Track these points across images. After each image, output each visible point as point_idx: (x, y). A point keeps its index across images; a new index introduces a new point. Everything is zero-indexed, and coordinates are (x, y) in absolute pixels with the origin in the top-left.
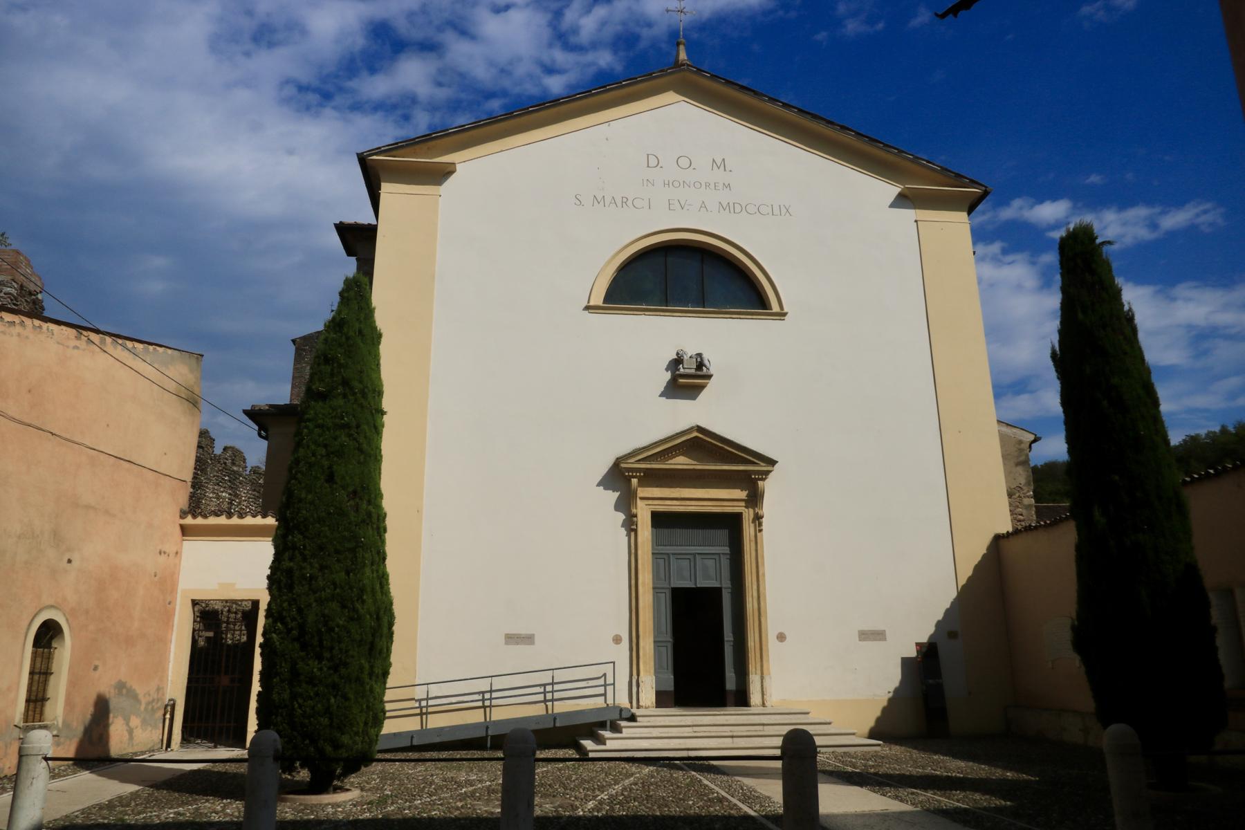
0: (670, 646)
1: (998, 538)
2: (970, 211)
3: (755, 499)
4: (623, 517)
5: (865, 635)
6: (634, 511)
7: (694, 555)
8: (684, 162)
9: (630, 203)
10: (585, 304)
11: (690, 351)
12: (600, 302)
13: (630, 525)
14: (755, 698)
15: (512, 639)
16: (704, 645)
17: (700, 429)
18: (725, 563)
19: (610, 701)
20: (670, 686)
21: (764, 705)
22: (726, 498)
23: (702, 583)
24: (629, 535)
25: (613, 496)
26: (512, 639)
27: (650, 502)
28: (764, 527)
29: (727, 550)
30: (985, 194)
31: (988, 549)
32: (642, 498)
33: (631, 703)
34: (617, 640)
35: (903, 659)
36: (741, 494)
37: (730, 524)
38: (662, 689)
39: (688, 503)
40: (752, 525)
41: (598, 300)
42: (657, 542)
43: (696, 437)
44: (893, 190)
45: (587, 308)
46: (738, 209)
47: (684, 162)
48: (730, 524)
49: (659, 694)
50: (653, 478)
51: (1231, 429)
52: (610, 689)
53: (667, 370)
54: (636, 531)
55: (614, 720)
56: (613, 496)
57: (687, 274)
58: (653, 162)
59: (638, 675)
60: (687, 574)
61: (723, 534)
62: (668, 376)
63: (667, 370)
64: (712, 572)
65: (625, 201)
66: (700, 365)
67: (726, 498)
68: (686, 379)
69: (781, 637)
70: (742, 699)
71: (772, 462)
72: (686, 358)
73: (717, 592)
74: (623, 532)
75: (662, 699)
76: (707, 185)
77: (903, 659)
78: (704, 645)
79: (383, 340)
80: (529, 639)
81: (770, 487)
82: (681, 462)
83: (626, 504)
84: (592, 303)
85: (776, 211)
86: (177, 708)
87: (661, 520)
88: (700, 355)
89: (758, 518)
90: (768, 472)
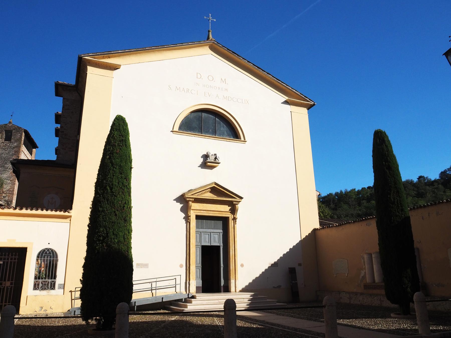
0: (200, 268)
1: (315, 230)
2: (308, 109)
3: (233, 211)
4: (184, 215)
7: (210, 233)
8: (211, 78)
9: (190, 91)
10: (172, 130)
11: (212, 153)
13: (187, 219)
14: (233, 289)
16: (214, 267)
17: (216, 184)
19: (178, 290)
20: (200, 285)
21: (236, 291)
24: (186, 223)
25: (180, 206)
27: (195, 211)
29: (221, 231)
30: (314, 105)
34: (181, 266)
36: (227, 208)
37: (225, 221)
38: (198, 286)
39: (209, 212)
40: (233, 221)
41: (176, 128)
42: (197, 227)
43: (214, 187)
44: (286, 98)
45: (172, 131)
46: (230, 99)
47: (211, 78)
48: (225, 221)
49: (197, 288)
50: (197, 201)
51: (344, 192)
53: (202, 157)
54: (190, 223)
55: (190, 298)
56: (180, 206)
57: (210, 122)
59: (189, 280)
61: (220, 223)
63: (202, 157)
64: (217, 240)
66: (216, 158)
67: (222, 210)
68: (207, 163)
71: (241, 198)
72: (210, 155)
73: (218, 247)
74: (184, 221)
76: (219, 88)
78: (214, 267)
81: (240, 207)
82: (209, 195)
83: (185, 210)
84: (174, 130)
85: (244, 102)
87: (198, 217)
88: (215, 154)
89: (234, 219)
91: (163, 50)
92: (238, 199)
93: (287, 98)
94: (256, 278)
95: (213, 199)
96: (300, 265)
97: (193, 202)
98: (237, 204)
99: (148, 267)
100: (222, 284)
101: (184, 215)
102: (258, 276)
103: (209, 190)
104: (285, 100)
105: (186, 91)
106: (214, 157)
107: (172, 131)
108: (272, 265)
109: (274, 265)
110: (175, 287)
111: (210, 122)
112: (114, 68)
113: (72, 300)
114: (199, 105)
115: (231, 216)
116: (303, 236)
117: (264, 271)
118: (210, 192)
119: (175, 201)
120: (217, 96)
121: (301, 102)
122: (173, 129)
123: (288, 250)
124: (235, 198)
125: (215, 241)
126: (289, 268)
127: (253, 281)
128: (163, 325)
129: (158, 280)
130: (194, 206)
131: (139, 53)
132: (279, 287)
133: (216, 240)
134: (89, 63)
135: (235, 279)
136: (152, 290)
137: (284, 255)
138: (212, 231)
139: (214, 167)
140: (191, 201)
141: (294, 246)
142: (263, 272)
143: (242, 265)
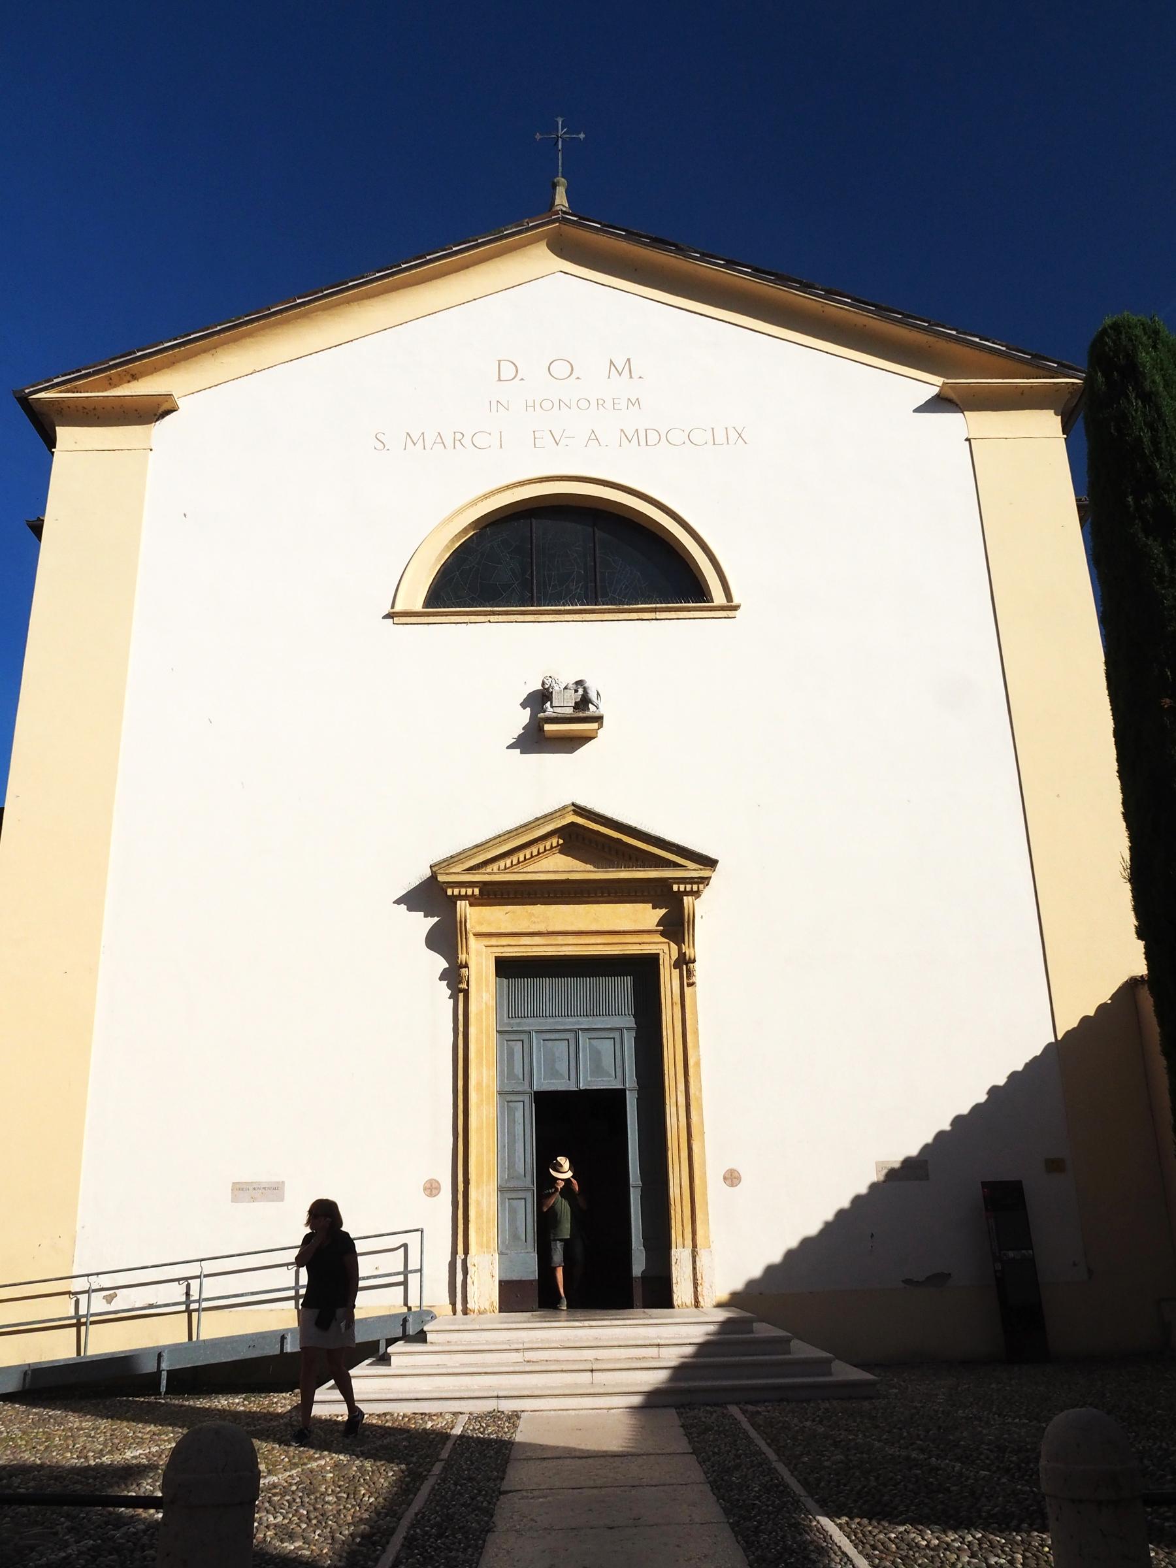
3: (676, 926)
4: (442, 964)
6: (689, 952)
7: (575, 1032)
8: (560, 369)
9: (467, 441)
10: (387, 609)
12: (418, 606)
13: (455, 978)
14: (682, 1291)
15: (243, 1191)
16: (593, 1191)
17: (579, 810)
18: (629, 1040)
20: (528, 1268)
21: (697, 1304)
22: (630, 924)
23: (588, 1081)
24: (454, 996)
25: (422, 923)
27: (494, 941)
28: (698, 977)
29: (630, 1022)
31: (1114, 997)
32: (477, 935)
33: (454, 1304)
34: (432, 1189)
35: (1020, 1182)
36: (648, 916)
37: (642, 973)
38: (515, 1277)
39: (560, 940)
40: (676, 972)
42: (509, 1007)
43: (572, 823)
44: (928, 385)
45: (390, 616)
47: (560, 369)
48: (642, 973)
52: (413, 1279)
53: (524, 705)
56: (422, 923)
57: (574, 551)
58: (508, 371)
59: (466, 1252)
60: (562, 1067)
61: (623, 988)
62: (525, 716)
63: (524, 705)
64: (608, 1062)
65: (459, 439)
66: (584, 702)
67: (630, 924)
68: (555, 724)
71: (711, 863)
73: (619, 1096)
75: (513, 1297)
76: (601, 403)
77: (1020, 1182)
78: (593, 1191)
83: (446, 939)
84: (399, 608)
85: (720, 437)
87: (506, 968)
88: (579, 683)
89: (684, 963)
90: (705, 880)
91: (348, 302)
92: (693, 870)
93: (939, 381)
94: (806, 1242)
95: (567, 881)
96: (1055, 1166)
97: (474, 902)
98: (697, 894)
99: (282, 1199)
100: (638, 1267)
101: (442, 964)
102: (813, 1228)
103: (554, 841)
104: (935, 391)
105: (449, 442)
106: (572, 698)
107: (390, 616)
108: (892, 1174)
109: (909, 1173)
110: (405, 1283)
111: (574, 551)
112: (155, 410)
113: (421, 1270)
114: (508, 487)
115: (667, 952)
116: (1068, 1022)
117: (845, 1203)
118: (565, 850)
119: (403, 907)
120: (594, 436)
121: (1016, 386)
122: (393, 607)
123: (982, 1098)
124: (676, 865)
125: (597, 1069)
126: (984, 1184)
127: (790, 1255)
128: (365, 1448)
129: (209, 1267)
130: (476, 917)
131: (250, 335)
132: (939, 1279)
133: (605, 1066)
134: (60, 412)
135: (694, 1246)
136: (78, 1325)
137: (958, 1121)
138: (585, 1023)
139: (585, 739)
140: (465, 897)
141: (1013, 1076)
142: (841, 1214)
143: (732, 1178)
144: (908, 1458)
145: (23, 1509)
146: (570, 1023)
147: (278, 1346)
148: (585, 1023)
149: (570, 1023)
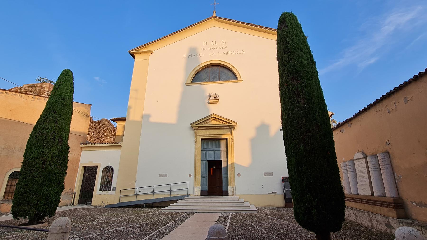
5: (265, 174)
14: (230, 193)
15: (161, 175)
20: (206, 188)
26: (161, 175)
34: (190, 176)
41: (189, 81)
47: (214, 43)
50: (200, 128)
57: (218, 71)
69: (136, 90)
70: (227, 194)
78: (215, 178)
79: (300, 20)
80: (166, 176)
86: (76, 194)
87: (202, 140)
138: (216, 149)
143: (239, 175)
144: (251, 225)
145: (42, 232)
146: (213, 149)
147: (362, 160)
148: (216, 149)
149: (213, 149)
